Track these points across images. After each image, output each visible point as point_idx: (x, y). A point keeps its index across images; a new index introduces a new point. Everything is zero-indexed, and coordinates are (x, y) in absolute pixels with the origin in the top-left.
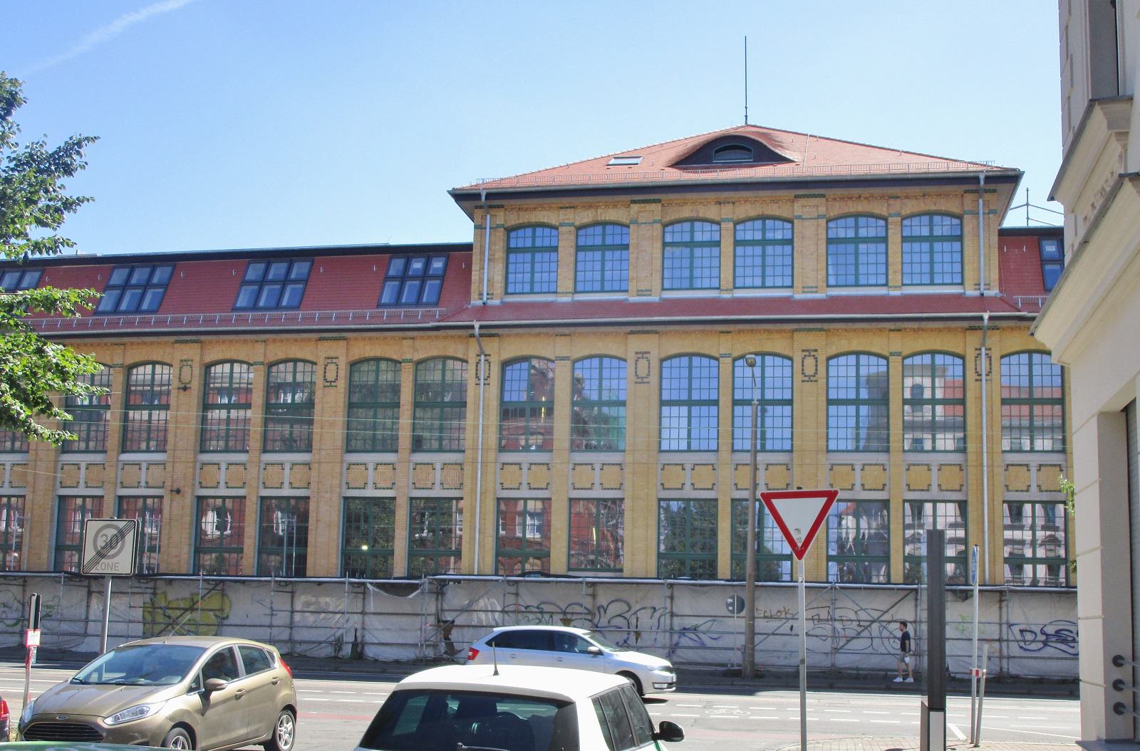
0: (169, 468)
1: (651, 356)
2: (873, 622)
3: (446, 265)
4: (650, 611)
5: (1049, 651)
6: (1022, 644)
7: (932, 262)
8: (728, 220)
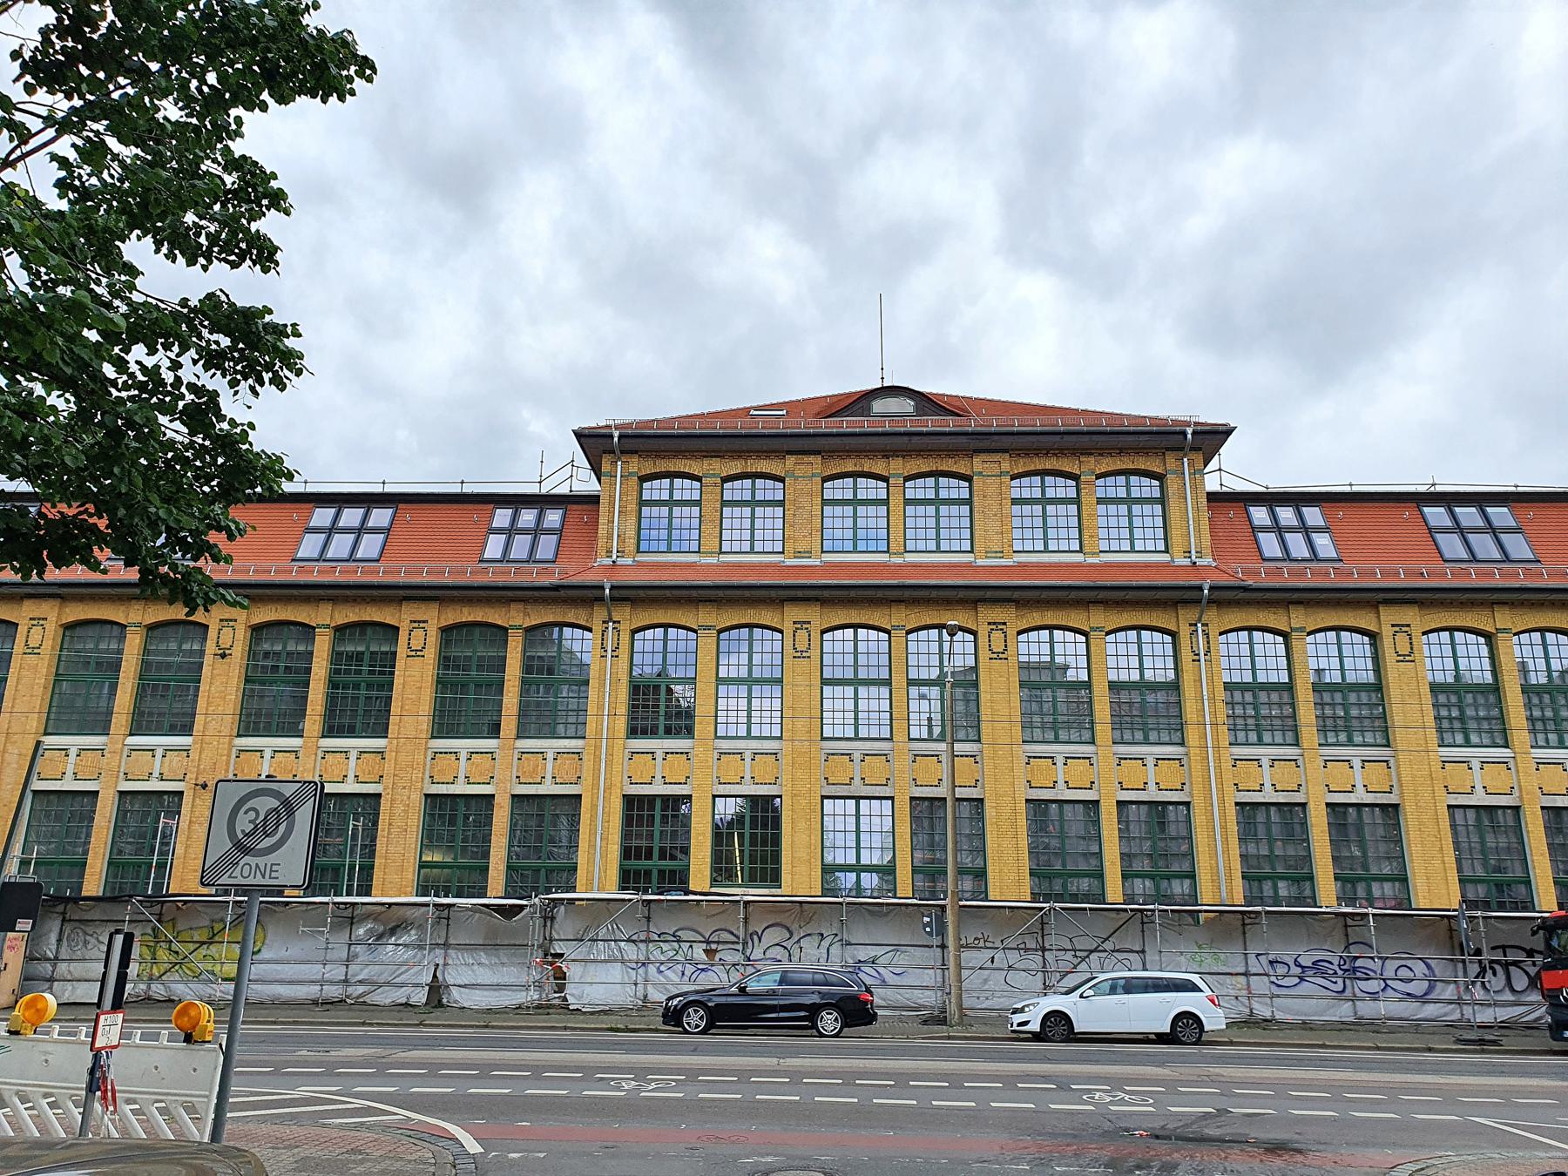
0: (194, 755)
1: (811, 627)
2: (1091, 952)
3: (564, 517)
4: (817, 939)
5: (1305, 988)
6: (1273, 979)
7: (1131, 528)
8: (898, 476)
